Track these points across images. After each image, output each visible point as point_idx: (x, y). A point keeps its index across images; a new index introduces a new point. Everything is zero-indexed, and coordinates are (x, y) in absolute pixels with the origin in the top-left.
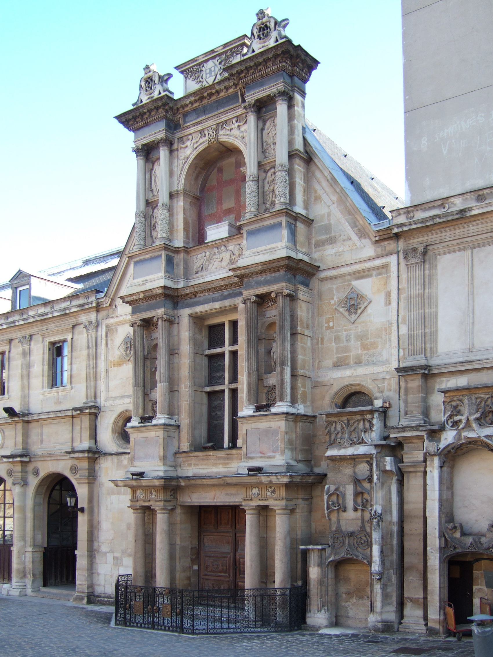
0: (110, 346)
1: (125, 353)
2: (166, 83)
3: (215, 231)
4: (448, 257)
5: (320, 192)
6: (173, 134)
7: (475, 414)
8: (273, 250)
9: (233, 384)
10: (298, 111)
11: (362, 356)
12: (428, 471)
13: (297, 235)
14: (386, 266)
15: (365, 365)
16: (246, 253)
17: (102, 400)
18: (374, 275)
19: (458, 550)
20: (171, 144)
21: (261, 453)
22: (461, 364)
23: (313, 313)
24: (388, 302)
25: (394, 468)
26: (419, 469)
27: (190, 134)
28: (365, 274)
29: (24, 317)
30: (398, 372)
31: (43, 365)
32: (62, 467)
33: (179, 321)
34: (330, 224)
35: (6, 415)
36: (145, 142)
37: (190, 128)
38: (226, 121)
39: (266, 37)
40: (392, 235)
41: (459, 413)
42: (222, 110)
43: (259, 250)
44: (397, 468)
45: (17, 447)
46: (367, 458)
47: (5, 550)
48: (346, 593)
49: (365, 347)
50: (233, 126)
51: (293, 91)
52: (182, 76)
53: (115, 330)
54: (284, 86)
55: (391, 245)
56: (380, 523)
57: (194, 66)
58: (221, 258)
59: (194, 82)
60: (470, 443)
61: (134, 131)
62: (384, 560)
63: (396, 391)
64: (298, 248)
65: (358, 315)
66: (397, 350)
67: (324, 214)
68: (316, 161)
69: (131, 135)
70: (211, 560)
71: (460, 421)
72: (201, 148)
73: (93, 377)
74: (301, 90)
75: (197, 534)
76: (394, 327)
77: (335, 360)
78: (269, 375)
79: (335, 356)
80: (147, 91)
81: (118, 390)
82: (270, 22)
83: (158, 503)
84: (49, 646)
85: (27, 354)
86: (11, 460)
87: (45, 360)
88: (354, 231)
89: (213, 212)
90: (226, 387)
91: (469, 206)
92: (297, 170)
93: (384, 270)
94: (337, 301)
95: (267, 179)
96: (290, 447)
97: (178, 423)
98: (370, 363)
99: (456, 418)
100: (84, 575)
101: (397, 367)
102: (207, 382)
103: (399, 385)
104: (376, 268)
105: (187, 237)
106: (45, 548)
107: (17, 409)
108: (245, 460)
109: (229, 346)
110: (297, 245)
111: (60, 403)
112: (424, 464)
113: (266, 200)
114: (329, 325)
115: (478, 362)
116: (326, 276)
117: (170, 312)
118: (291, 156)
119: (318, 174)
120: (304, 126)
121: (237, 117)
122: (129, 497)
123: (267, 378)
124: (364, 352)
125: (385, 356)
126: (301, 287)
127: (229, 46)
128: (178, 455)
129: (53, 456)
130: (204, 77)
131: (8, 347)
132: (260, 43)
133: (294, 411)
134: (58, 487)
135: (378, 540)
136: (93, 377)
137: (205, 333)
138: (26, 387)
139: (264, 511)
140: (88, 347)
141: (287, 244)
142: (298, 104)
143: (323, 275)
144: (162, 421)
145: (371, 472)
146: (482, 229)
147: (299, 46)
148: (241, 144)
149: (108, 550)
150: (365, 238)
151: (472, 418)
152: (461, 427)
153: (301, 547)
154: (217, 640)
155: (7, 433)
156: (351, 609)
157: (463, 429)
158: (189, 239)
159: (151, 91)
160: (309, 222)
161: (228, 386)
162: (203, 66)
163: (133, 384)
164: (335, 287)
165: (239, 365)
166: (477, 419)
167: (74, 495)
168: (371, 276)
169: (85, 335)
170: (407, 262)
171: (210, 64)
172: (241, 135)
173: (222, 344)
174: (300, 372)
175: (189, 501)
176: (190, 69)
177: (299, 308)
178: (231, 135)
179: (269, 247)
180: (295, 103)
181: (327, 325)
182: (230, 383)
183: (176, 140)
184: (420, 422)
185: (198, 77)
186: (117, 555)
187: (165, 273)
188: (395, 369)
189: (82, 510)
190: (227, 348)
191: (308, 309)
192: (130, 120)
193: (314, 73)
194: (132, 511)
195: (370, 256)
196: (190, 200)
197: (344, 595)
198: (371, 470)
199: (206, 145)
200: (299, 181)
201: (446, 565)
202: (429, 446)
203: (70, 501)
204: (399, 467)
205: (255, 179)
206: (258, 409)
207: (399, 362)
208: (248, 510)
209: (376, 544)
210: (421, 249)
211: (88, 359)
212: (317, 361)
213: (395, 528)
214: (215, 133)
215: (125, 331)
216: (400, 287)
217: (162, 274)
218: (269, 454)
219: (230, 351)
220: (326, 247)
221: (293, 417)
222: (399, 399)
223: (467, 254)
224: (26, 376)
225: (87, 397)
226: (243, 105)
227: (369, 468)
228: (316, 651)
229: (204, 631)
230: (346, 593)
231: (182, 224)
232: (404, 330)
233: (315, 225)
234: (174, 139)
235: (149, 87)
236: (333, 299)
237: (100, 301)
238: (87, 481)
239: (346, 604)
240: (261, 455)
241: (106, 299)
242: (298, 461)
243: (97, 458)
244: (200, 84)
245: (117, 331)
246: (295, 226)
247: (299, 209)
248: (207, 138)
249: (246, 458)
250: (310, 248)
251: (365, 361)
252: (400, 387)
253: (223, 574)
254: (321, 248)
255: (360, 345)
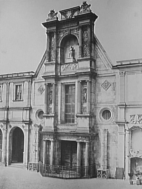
61: (47, 27)
73: (29, 98)
81: (39, 102)
136: (29, 98)
176: (63, 13)
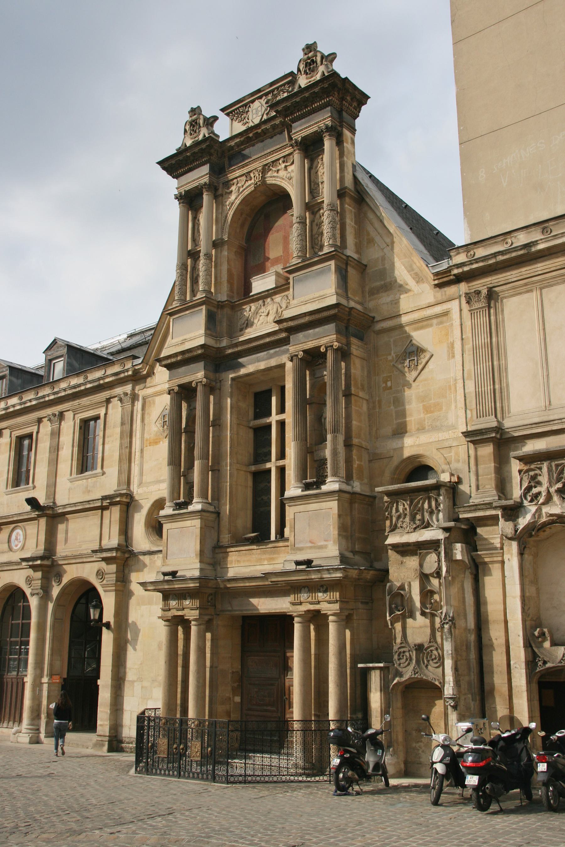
0: (146, 421)
1: (162, 428)
2: (212, 126)
3: (260, 282)
4: (515, 299)
5: (373, 234)
6: (218, 178)
7: (556, 483)
8: (323, 297)
9: (281, 461)
10: (347, 148)
11: (425, 420)
12: (506, 560)
13: (349, 281)
14: (446, 314)
15: (429, 431)
16: (293, 303)
17: (135, 486)
18: (434, 324)
19: (549, 665)
20: (216, 189)
21: (311, 542)
22: (537, 425)
23: (369, 372)
24: (452, 355)
25: (466, 557)
26: (495, 559)
27: (236, 178)
28: (425, 323)
29: (56, 390)
30: (465, 436)
31: (73, 446)
32: (88, 572)
33: (220, 386)
34: (385, 269)
35: (28, 508)
36: (187, 189)
37: (235, 171)
38: (273, 162)
39: (313, 71)
40: (452, 277)
41: (539, 483)
42: (269, 151)
43: (307, 299)
44: (469, 558)
45: (39, 548)
46: (433, 545)
47: (18, 683)
48: (416, 730)
49: (427, 410)
50: (280, 167)
51: (342, 126)
52: (228, 119)
53: (152, 402)
54: (331, 120)
55: (452, 290)
56: (453, 630)
57: (240, 107)
58: (267, 312)
59: (241, 124)
60: (552, 522)
62: (459, 681)
63: (465, 461)
64: (350, 295)
65: (418, 372)
66: (464, 412)
67: (378, 258)
68: (368, 200)
69: (174, 182)
70: (256, 690)
71: (539, 493)
72: (246, 192)
73: (127, 458)
74: (350, 126)
75: (239, 654)
76: (460, 384)
77: (394, 426)
78: (320, 446)
79: (395, 422)
80: (191, 134)
82: (316, 56)
83: (193, 612)
84: (47, 795)
85: (56, 434)
86: (31, 563)
87: (75, 441)
88: (411, 275)
89: (260, 262)
90: (272, 465)
91: (533, 240)
92: (347, 210)
93: (445, 318)
94: (394, 357)
95: (316, 221)
96: (344, 534)
97: (217, 509)
98: (435, 428)
99: (535, 491)
100: (107, 713)
101: (465, 430)
102: (252, 460)
103: (469, 454)
104: (437, 316)
105: (231, 290)
106: (64, 679)
107: (42, 501)
108: (293, 552)
109: (277, 415)
110: (349, 293)
111: (89, 491)
112: (502, 551)
113: (315, 244)
114: (386, 384)
115: (556, 422)
116: (382, 327)
117: (211, 375)
118: (341, 194)
119: (371, 215)
120: (355, 164)
121: (284, 157)
122: (161, 604)
123: (318, 450)
124: (426, 416)
125: (451, 418)
126: (354, 340)
127: (275, 84)
128: (217, 551)
129: (78, 559)
130: (250, 118)
131: (36, 427)
132: (307, 79)
133: (348, 488)
134: (83, 601)
135: (450, 652)
137: (251, 400)
138: (53, 474)
139: (316, 618)
140: (123, 424)
141: (338, 290)
142: (347, 139)
143: (379, 326)
144: (199, 507)
145: (439, 564)
146: (550, 266)
147: (346, 78)
148: (288, 185)
149: (135, 679)
150: (423, 283)
151: (552, 490)
152: (541, 501)
153: (360, 665)
154: (256, 790)
155: (29, 532)
156: (423, 751)
157: (543, 504)
158: (233, 293)
159: (195, 135)
160: (362, 268)
161: (276, 463)
162: (250, 106)
163: (169, 462)
164: (392, 340)
165: (286, 436)
166: (559, 491)
167: (99, 605)
168: (431, 325)
169: (120, 409)
170: (470, 307)
171: (257, 103)
172: (288, 175)
173: (270, 415)
174: (355, 441)
175: (230, 608)
176: (234, 110)
177: (352, 365)
178: (277, 177)
179: (317, 295)
180: (344, 139)
181: (384, 385)
182: (277, 460)
183: (221, 185)
184: (494, 498)
185: (245, 119)
186: (146, 684)
187: (205, 331)
188: (462, 433)
189: (108, 625)
190: (274, 418)
191: (363, 367)
192: (174, 165)
193: (364, 108)
194: (164, 623)
195: (429, 303)
196: (234, 250)
197: (414, 732)
198: (439, 561)
199: (252, 188)
200: (350, 222)
201: (535, 686)
202: (505, 526)
203: (93, 614)
204: (472, 557)
205: (302, 221)
206: (307, 487)
207: (467, 425)
208: (297, 616)
209: (448, 659)
210: (484, 292)
211: (121, 438)
212: (374, 429)
213: (472, 638)
214: (261, 175)
215: (164, 402)
216: (464, 337)
217: (202, 331)
218: (320, 544)
219: (277, 421)
220: (381, 295)
221: (347, 496)
222: (469, 472)
223: (534, 296)
224: (54, 462)
225: (119, 484)
226: (289, 144)
227: (437, 558)
228: (376, 802)
229: (241, 778)
230: (416, 730)
231: (226, 276)
232: (471, 387)
233: (369, 271)
234: (219, 183)
235: (193, 130)
236: (390, 354)
237: (136, 368)
238: (114, 588)
239: (417, 745)
240: (310, 545)
241: (143, 366)
242: (354, 552)
243: (127, 558)
244: (246, 126)
245: (154, 403)
246: (346, 271)
247: (350, 252)
248: (253, 181)
249: (294, 550)
250: (364, 297)
251: (429, 426)
252: (469, 457)
253: (269, 708)
254: (376, 296)
255: (421, 407)
